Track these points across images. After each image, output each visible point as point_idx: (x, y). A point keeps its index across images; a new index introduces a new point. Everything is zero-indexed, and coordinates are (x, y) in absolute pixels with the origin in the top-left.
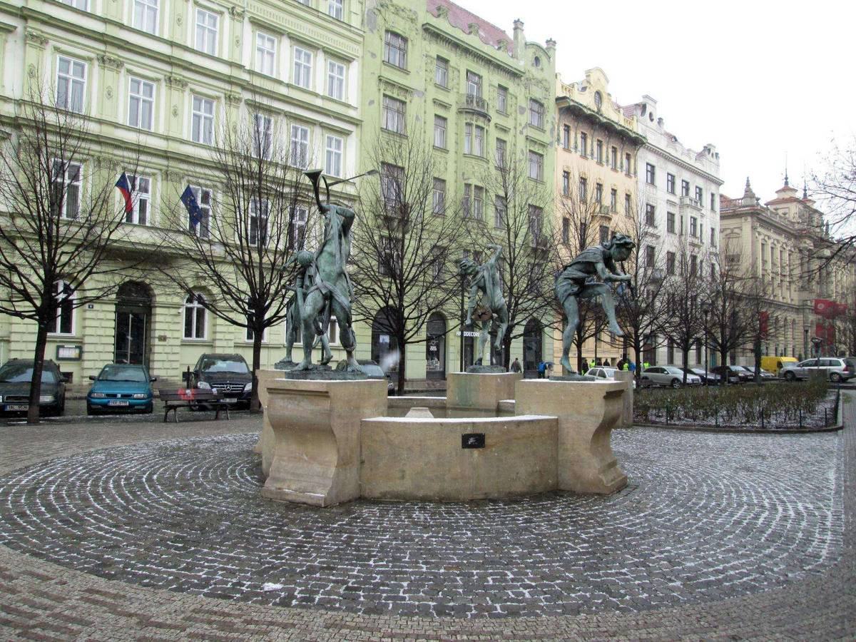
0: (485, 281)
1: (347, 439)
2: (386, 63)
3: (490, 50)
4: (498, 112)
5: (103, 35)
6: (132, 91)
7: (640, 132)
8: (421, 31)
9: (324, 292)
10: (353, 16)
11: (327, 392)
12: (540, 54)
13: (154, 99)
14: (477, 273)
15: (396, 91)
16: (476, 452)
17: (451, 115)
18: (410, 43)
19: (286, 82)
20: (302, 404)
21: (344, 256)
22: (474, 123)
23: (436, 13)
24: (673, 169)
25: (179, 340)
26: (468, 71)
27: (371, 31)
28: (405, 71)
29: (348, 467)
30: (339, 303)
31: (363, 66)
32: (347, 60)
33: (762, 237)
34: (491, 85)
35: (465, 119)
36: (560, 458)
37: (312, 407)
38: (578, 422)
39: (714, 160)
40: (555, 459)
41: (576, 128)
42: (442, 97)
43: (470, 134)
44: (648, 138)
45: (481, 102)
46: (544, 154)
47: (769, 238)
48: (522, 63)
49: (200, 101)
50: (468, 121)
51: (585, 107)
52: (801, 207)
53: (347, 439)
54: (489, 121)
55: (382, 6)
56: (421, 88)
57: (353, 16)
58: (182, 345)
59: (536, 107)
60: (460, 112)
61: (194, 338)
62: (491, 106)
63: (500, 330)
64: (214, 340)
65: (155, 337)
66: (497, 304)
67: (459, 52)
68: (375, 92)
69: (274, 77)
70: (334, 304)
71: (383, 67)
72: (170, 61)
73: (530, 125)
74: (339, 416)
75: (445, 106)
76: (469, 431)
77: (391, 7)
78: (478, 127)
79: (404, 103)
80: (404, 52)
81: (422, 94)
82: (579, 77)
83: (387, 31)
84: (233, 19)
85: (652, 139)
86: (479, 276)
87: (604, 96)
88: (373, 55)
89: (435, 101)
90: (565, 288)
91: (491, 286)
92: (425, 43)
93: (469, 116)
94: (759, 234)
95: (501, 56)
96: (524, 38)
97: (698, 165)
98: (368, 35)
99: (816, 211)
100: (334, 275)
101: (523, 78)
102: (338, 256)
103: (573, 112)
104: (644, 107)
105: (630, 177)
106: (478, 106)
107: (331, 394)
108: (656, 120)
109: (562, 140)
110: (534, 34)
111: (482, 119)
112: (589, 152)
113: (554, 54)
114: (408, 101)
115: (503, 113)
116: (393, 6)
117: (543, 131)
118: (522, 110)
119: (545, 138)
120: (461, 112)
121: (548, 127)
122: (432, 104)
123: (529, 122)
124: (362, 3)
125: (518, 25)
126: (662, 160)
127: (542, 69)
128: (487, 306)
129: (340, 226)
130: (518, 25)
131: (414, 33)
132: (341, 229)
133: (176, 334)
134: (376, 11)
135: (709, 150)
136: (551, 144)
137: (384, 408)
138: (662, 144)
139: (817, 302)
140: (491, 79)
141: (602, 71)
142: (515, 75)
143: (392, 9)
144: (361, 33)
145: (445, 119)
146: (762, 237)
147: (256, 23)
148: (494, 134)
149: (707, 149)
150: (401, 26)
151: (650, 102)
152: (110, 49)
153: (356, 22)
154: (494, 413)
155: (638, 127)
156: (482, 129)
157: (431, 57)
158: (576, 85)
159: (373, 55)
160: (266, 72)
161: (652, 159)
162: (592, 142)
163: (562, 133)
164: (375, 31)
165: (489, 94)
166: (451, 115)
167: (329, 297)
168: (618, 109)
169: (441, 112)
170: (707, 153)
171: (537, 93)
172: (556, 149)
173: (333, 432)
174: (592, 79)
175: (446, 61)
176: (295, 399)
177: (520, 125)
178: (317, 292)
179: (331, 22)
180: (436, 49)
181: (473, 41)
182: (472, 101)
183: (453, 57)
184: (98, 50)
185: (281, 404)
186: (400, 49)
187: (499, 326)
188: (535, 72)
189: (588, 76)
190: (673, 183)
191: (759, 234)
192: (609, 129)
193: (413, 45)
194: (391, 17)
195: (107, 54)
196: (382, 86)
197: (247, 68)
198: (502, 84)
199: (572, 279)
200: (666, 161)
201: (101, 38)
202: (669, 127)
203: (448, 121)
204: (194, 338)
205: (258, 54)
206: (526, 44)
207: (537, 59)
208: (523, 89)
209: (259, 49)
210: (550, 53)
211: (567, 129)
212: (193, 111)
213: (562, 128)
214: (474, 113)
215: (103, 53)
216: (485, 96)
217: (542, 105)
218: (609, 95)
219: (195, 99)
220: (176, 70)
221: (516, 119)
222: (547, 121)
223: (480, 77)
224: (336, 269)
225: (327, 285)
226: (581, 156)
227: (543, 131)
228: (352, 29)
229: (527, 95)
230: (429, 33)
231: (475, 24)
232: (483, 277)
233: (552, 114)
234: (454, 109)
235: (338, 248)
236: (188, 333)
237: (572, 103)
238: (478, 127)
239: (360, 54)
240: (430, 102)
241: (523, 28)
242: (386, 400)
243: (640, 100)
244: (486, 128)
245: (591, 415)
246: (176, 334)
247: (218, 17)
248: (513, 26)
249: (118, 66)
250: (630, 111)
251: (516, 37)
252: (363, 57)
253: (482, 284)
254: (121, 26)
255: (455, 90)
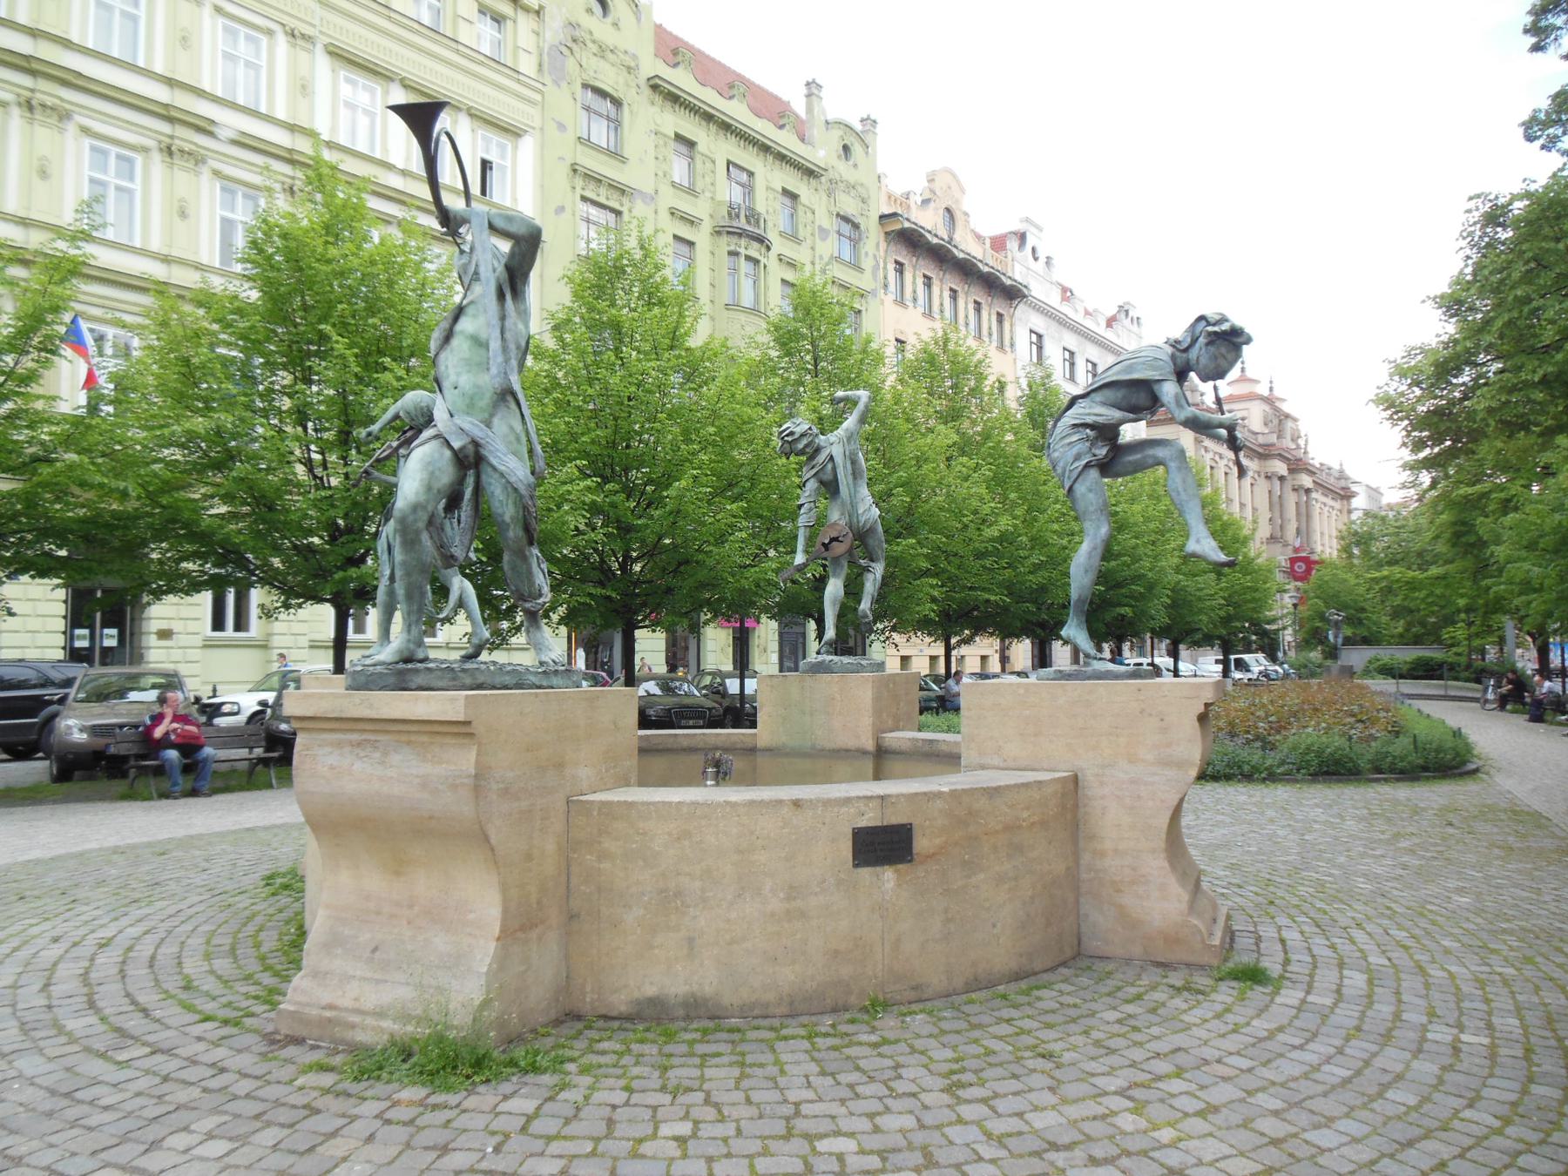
0: (834, 469)
1: (529, 857)
2: (585, 142)
3: (763, 128)
4: (781, 234)
5: (28, 58)
6: (92, 168)
7: (1018, 277)
8: (647, 91)
9: (456, 445)
10: (523, 56)
11: (467, 723)
12: (851, 140)
13: (137, 186)
14: (818, 450)
15: (603, 191)
16: (888, 876)
17: (702, 237)
18: (626, 108)
19: (400, 166)
20: (395, 758)
21: (512, 346)
22: (742, 251)
23: (672, 60)
24: (1071, 341)
25: (200, 637)
26: (729, 163)
27: (556, 83)
28: (616, 155)
29: (534, 934)
30: (502, 475)
31: (542, 146)
32: (512, 132)
33: (1210, 455)
34: (768, 188)
35: (726, 244)
36: (1084, 876)
37: (427, 769)
38: (1133, 782)
39: (1135, 328)
40: (1073, 878)
41: (914, 267)
42: (686, 205)
43: (734, 270)
44: (1031, 287)
45: (753, 217)
46: (863, 309)
47: (1221, 458)
48: (821, 153)
49: (233, 193)
50: (732, 248)
51: (930, 232)
52: (1267, 408)
53: (529, 857)
54: (768, 248)
55: (574, 41)
56: (648, 188)
57: (523, 56)
58: (205, 646)
59: (846, 228)
60: (717, 232)
61: (229, 631)
62: (770, 224)
63: (870, 577)
64: (270, 635)
65: (150, 633)
66: (863, 520)
67: (713, 128)
68: (564, 189)
69: (378, 155)
70: (484, 477)
71: (579, 147)
72: (167, 114)
73: (838, 259)
74: (505, 792)
75: (691, 221)
76: (869, 819)
77: (590, 45)
78: (748, 258)
79: (618, 213)
80: (616, 124)
81: (651, 198)
82: (918, 186)
83: (585, 86)
84: (294, 46)
85: (1039, 290)
86: (822, 457)
87: (958, 215)
88: (562, 127)
89: (672, 213)
90: (1075, 450)
91: (850, 478)
92: (656, 109)
93: (735, 239)
94: (1206, 450)
95: (785, 140)
96: (824, 113)
97: (1109, 335)
98: (550, 89)
99: (1287, 416)
100: (485, 401)
101: (823, 179)
102: (495, 345)
103: (911, 240)
104: (1022, 237)
105: (1005, 352)
106: (749, 222)
107: (478, 728)
108: (1042, 260)
109: (892, 287)
110: (840, 105)
111: (756, 245)
112: (936, 308)
113: (875, 140)
114: (625, 210)
115: (793, 237)
116: (594, 42)
117: (860, 269)
118: (824, 233)
119: (864, 281)
120: (719, 233)
121: (867, 264)
122: (668, 216)
123: (836, 254)
124: (538, 34)
125: (812, 89)
126: (1054, 325)
127: (855, 166)
128: (842, 522)
129: (500, 269)
130: (812, 89)
131: (634, 91)
132: (505, 276)
133: (192, 627)
134: (564, 50)
135: (1127, 312)
136: (873, 293)
137: (632, 762)
138: (1054, 299)
139: (1293, 561)
140: (771, 177)
141: (954, 176)
142: (810, 173)
143: (594, 48)
144: (540, 86)
145: (691, 244)
146: (1210, 455)
147: (339, 56)
148: (776, 272)
149: (1124, 310)
150: (609, 79)
151: (1033, 230)
152: (43, 85)
153: (527, 66)
154: (868, 765)
155: (1018, 269)
156: (756, 262)
157: (665, 136)
158: (911, 196)
159: (562, 127)
160: (362, 147)
161: (1039, 323)
162: (941, 292)
163: (892, 275)
164: (564, 84)
165: (765, 202)
166: (702, 237)
167: (470, 460)
168: (978, 237)
169: (685, 232)
170: (1123, 315)
171: (849, 206)
172: (882, 302)
173: (487, 839)
174: (937, 186)
175: (691, 144)
176: (374, 745)
177: (821, 258)
178: (435, 444)
179: (481, 63)
180: (675, 121)
181: (737, 111)
182: (738, 216)
183: (703, 136)
184: (19, 86)
185: (333, 759)
186: (608, 118)
187: (867, 569)
188: (842, 169)
189: (931, 181)
190: (1072, 364)
191: (1206, 450)
192: (966, 270)
193: (631, 112)
194: (592, 63)
195: (38, 95)
196: (579, 182)
197: (325, 137)
198: (789, 188)
199: (1092, 426)
200: (1061, 327)
201: (25, 64)
202: (1061, 274)
203: (698, 246)
204: (229, 631)
205: (343, 113)
206: (827, 123)
207: (846, 148)
208: (825, 197)
209: (348, 105)
210: (868, 139)
211: (900, 267)
212: (219, 212)
213: (891, 267)
214: (741, 234)
215: (28, 94)
216: (760, 207)
217: (856, 226)
218: (966, 214)
219: (223, 189)
220: (181, 131)
221: (813, 249)
222: (867, 254)
223: (751, 174)
224: (489, 381)
225: (466, 426)
226: (924, 314)
227: (860, 269)
228: (521, 77)
229: (832, 209)
230: (661, 93)
231: (733, 84)
232: (832, 458)
233: (874, 241)
234: (707, 226)
235: (495, 321)
236: (218, 624)
237: (907, 225)
238: (748, 258)
239: (537, 123)
240: (664, 216)
241: (822, 94)
242: (636, 739)
243: (1020, 227)
244: (763, 260)
245: (1166, 763)
246: (192, 627)
247: (264, 40)
248: (804, 91)
249: (61, 119)
250: (998, 243)
251: (809, 109)
252: (542, 129)
253: (827, 476)
254: (66, 44)
255: (708, 194)
